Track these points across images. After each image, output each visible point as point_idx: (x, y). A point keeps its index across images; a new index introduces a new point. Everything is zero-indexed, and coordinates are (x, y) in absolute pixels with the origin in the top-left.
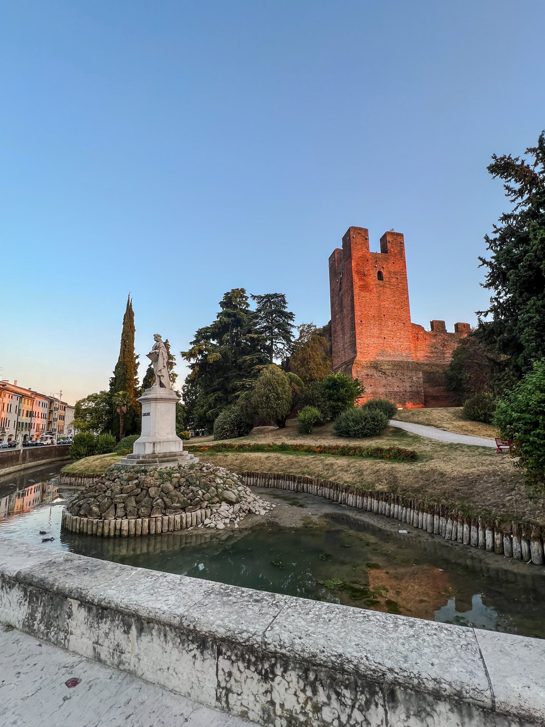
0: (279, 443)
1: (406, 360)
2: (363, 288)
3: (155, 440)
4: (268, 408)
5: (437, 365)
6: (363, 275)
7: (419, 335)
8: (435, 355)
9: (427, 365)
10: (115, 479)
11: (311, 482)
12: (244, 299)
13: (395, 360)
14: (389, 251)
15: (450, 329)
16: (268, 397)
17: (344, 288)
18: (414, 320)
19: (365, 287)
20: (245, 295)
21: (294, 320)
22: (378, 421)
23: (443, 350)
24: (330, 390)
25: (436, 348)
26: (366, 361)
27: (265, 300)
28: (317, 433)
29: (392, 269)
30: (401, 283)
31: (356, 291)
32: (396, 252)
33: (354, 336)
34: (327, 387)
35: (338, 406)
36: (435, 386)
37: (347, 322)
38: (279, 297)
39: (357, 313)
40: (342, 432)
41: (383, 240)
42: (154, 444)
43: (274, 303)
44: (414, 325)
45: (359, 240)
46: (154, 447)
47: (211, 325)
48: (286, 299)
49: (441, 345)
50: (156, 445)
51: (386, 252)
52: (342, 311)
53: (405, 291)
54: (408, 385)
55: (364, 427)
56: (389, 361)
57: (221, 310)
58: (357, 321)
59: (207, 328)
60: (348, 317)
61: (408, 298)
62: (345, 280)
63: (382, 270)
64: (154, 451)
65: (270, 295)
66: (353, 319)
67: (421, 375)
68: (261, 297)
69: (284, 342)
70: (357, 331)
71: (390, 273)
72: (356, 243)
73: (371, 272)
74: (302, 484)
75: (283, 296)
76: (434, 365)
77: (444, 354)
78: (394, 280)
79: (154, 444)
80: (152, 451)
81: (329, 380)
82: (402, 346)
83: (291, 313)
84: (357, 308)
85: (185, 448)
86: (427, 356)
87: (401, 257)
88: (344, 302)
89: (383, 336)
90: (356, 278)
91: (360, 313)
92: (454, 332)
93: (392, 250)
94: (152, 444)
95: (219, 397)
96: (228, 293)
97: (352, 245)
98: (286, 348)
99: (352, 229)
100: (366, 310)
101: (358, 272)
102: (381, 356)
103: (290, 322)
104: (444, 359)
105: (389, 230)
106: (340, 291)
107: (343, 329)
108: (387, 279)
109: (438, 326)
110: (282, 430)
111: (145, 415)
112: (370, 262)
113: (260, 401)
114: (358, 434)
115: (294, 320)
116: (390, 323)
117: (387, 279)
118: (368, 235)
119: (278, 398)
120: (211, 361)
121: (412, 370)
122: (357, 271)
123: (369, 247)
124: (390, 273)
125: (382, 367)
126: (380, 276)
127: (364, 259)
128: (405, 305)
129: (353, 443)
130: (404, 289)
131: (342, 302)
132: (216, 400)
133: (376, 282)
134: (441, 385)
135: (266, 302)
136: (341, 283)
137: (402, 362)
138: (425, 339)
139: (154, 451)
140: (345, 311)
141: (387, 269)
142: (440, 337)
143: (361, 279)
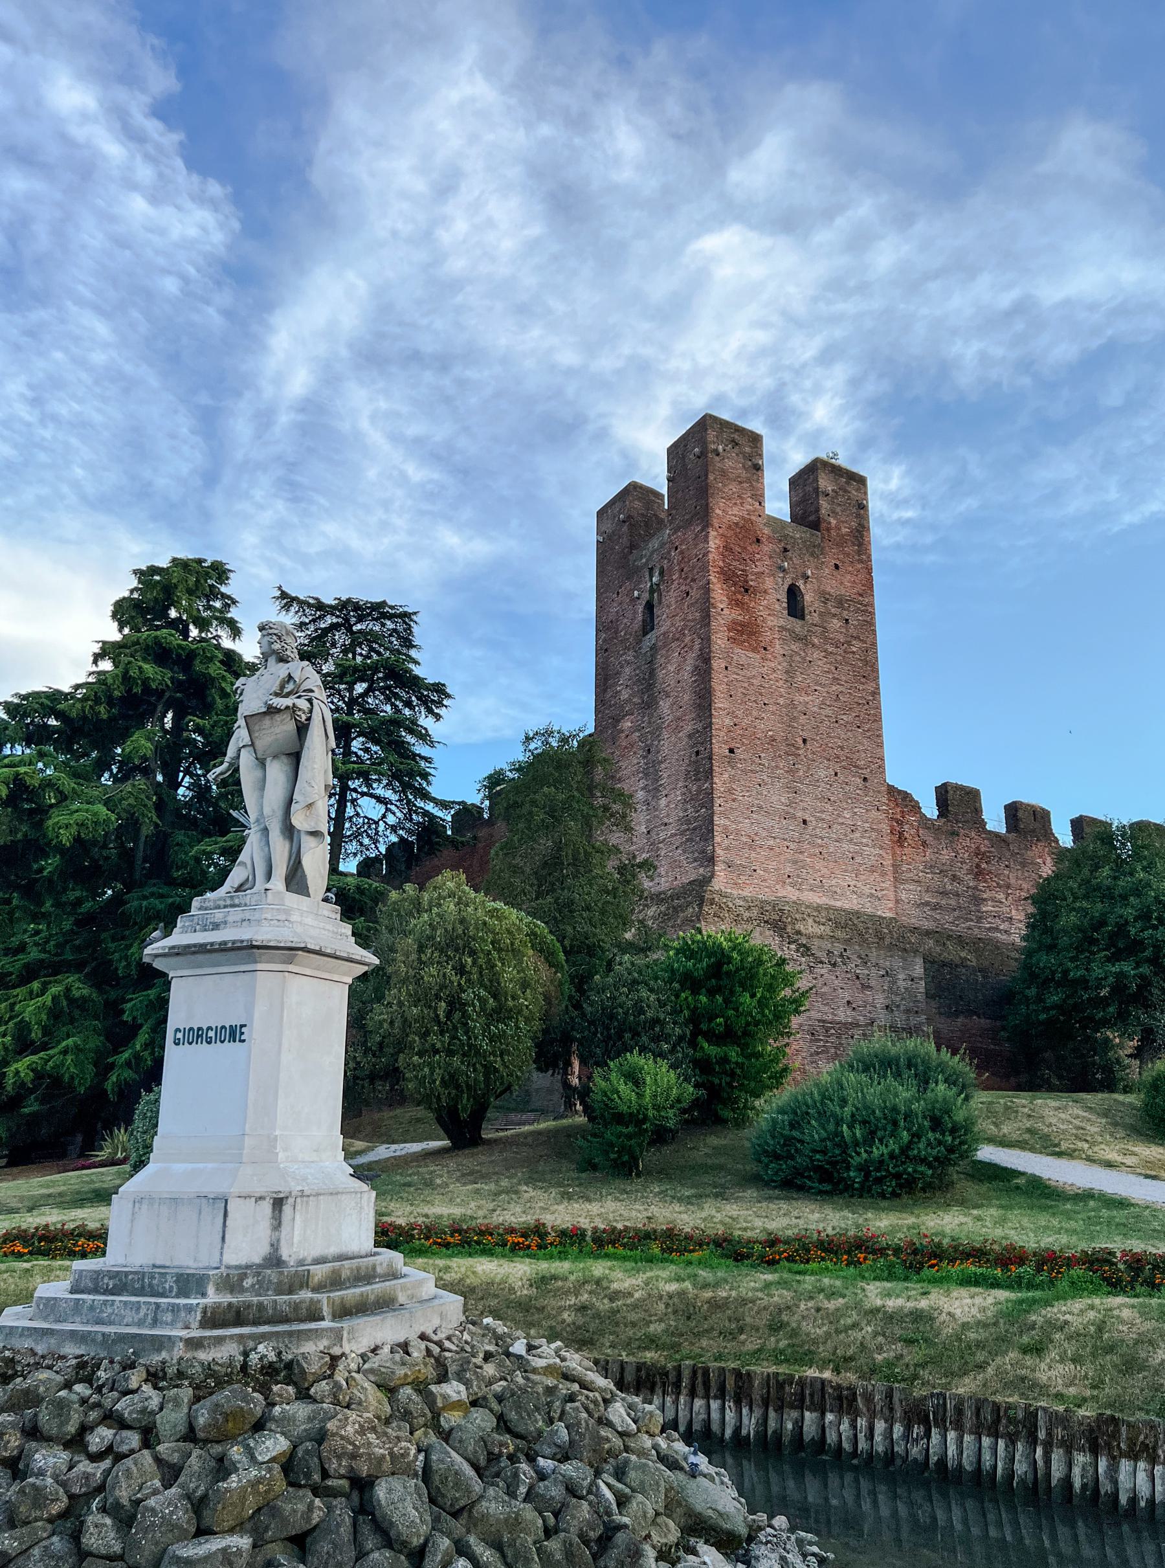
0: (514, 1215)
1: (869, 910)
2: (741, 633)
3: (283, 1188)
4: (450, 1053)
5: (960, 940)
6: (743, 589)
7: (906, 827)
8: (953, 902)
9: (928, 933)
10: (85, 1429)
11: (846, 1402)
12: (218, 604)
13: (838, 904)
14: (823, 525)
15: (995, 820)
16: (455, 1004)
17: (665, 623)
18: (895, 777)
19: (746, 632)
20: (223, 589)
21: (438, 717)
22: (953, 1131)
23: (975, 888)
24: (695, 992)
25: (954, 878)
26: (744, 899)
27: (330, 620)
28: (663, 1173)
29: (832, 586)
30: (857, 638)
31: (720, 640)
32: (845, 530)
33: (706, 800)
34: (691, 982)
35: (725, 1060)
36: (957, 1014)
37: (673, 747)
38: (391, 617)
39: (721, 720)
40: (798, 1173)
41: (805, 483)
42: (278, 1203)
43: (370, 638)
44: (891, 790)
45: (732, 463)
46: (277, 1225)
47: (77, 687)
48: (415, 629)
49: (970, 872)
50: (287, 1209)
51: (815, 525)
52: (649, 705)
53: (868, 670)
54: (880, 1000)
55: (905, 1150)
56: (818, 909)
57: (112, 633)
58: (719, 748)
59: (55, 696)
60: (678, 729)
61: (876, 693)
62: (671, 597)
63: (800, 583)
64: (275, 1246)
65: (357, 607)
66: (702, 736)
67: (918, 969)
68: (320, 606)
69: (389, 794)
70: (720, 781)
71: (825, 597)
72: (724, 473)
73: (769, 583)
74: (795, 1414)
75: (405, 616)
76: (949, 937)
77: (978, 901)
78: (836, 623)
79: (278, 1203)
80: (264, 1250)
81: (686, 951)
82: (858, 859)
83: (439, 689)
84: (720, 703)
85: (388, 1236)
86: (927, 904)
87: (859, 553)
88: (661, 674)
89: (799, 814)
90: (719, 594)
91: (728, 721)
92: (1002, 829)
93: (833, 522)
94: (267, 1207)
95: (72, 1001)
96: (153, 570)
97: (711, 477)
98: (391, 819)
99: (706, 425)
100: (748, 713)
101: (728, 576)
102: (793, 885)
103: (425, 721)
104: (979, 919)
105: (823, 456)
106: (645, 634)
107: (651, 772)
108: (816, 618)
109: (957, 802)
110: (469, 1160)
111: (198, 1035)
112: (767, 548)
113: (420, 1019)
114: (879, 1181)
115: (438, 717)
116: (822, 773)
117: (816, 618)
118: (761, 456)
119: (501, 1013)
120: (66, 837)
121: (891, 947)
122: (722, 572)
123: (762, 495)
124: (825, 597)
125: (800, 926)
126: (794, 604)
127: (747, 534)
128: (866, 714)
129: (886, 1223)
130: (866, 663)
131: (652, 673)
132: (55, 1013)
133: (782, 622)
134: (975, 1013)
135: (334, 627)
136: (650, 607)
137: (857, 914)
138: (924, 844)
139: (275, 1246)
140: (664, 705)
141: (822, 582)
142: (968, 842)
143: (736, 603)
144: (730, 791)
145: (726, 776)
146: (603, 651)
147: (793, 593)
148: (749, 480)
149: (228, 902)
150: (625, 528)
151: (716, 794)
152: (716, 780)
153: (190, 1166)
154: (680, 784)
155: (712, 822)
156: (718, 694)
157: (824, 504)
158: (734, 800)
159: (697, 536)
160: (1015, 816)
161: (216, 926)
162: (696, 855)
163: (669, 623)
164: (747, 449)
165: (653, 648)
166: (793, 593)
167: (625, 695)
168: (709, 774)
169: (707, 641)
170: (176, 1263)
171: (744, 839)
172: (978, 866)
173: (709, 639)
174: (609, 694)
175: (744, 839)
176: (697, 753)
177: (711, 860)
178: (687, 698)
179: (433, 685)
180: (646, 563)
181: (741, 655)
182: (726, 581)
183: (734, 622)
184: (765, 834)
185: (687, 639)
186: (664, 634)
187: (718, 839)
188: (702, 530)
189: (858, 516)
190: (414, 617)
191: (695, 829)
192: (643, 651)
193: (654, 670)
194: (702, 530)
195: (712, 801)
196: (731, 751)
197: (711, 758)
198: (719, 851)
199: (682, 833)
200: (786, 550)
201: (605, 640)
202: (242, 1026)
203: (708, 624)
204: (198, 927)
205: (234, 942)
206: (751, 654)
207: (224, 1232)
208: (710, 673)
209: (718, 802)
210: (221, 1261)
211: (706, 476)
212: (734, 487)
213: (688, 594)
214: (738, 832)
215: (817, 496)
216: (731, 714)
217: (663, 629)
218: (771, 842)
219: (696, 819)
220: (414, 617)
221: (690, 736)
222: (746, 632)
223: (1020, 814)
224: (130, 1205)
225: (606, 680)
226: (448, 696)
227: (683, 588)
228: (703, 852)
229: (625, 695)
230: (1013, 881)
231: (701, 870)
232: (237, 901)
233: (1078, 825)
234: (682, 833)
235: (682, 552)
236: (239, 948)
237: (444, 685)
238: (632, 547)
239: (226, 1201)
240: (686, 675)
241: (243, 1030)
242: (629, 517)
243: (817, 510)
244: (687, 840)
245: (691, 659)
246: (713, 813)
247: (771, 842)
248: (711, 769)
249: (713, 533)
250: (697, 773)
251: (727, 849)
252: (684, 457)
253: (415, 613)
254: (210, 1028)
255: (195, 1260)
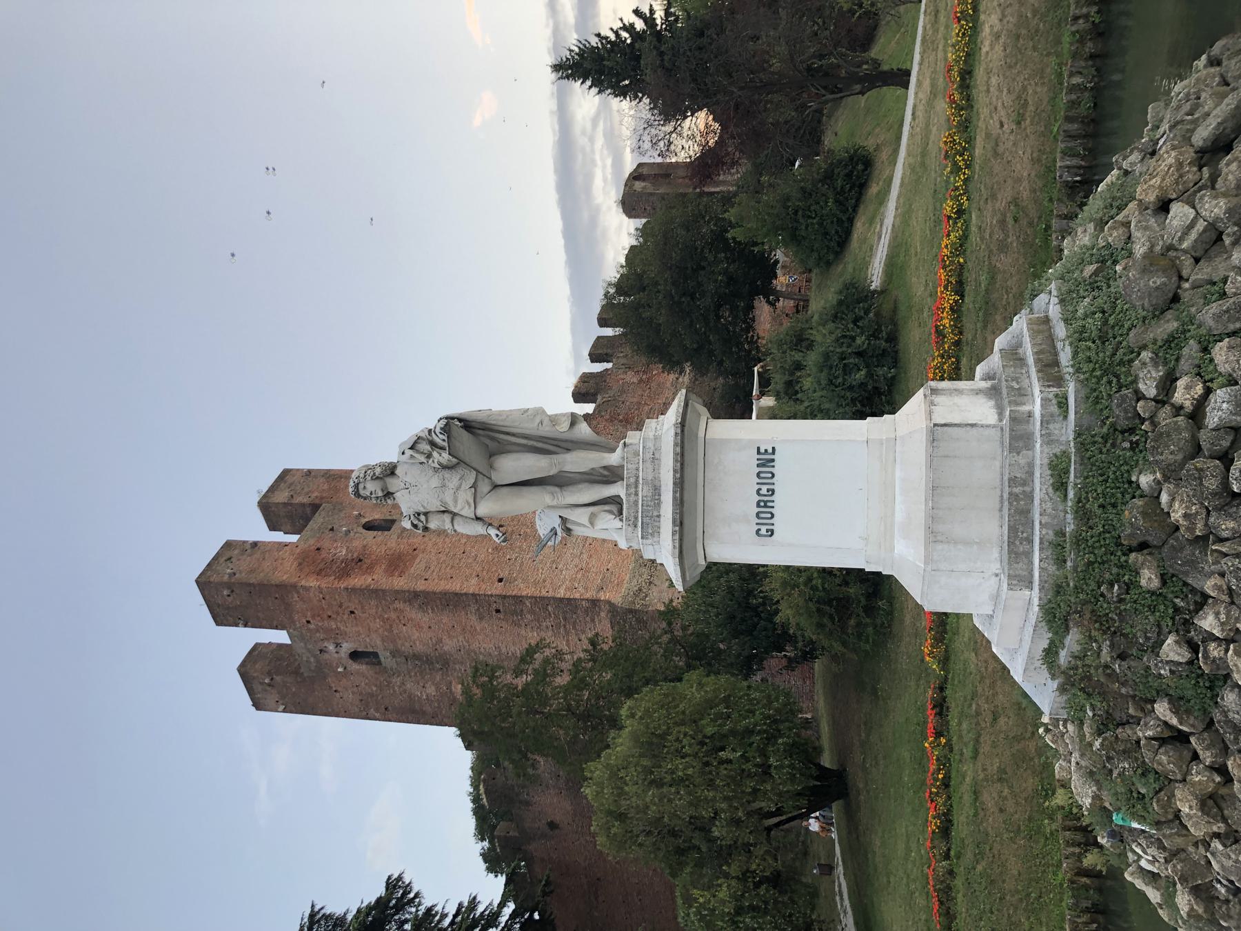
14: (317, 502)
31: (399, 583)
33: (542, 602)
39: (472, 586)
58: (498, 589)
63: (364, 521)
73: (357, 544)
83: (393, 884)
84: (455, 586)
88: (419, 648)
91: (474, 581)
93: (316, 494)
112: (326, 544)
122: (340, 578)
131: (416, 657)
140: (449, 645)
143: (370, 569)
144: (536, 583)
145: (522, 586)
146: (388, 714)
147: (369, 527)
148: (264, 553)
149: (633, 490)
150: (278, 678)
151: (537, 594)
152: (524, 593)
153: (898, 498)
154: (523, 632)
155: (561, 600)
156: (448, 587)
157: (299, 499)
158: (544, 581)
159: (302, 599)
160: (584, 395)
161: (657, 490)
162: (588, 619)
163: (374, 636)
164: (236, 552)
165: (395, 653)
166: (369, 527)
167: (431, 690)
168: (518, 599)
169: (398, 594)
170: (998, 483)
171: (579, 576)
172: (621, 421)
173: (397, 592)
174: (428, 709)
175: (579, 576)
176: (498, 611)
177: (595, 602)
178: (446, 619)
179: (387, 889)
180: (315, 656)
181: (417, 567)
182: (348, 575)
183: (386, 571)
184: (577, 560)
185: (393, 615)
186: (383, 641)
187: (577, 596)
188: (298, 592)
189: (316, 477)
190: (316, 909)
191: (565, 619)
192: (395, 666)
193: (414, 655)
194: (298, 592)
195: (542, 598)
196: (500, 580)
197: (505, 597)
198: (588, 596)
199: (567, 633)
200: (332, 529)
201: (377, 710)
202: (759, 452)
203: (383, 591)
204: (655, 513)
205: (675, 471)
206: (418, 560)
207: (967, 425)
208: (428, 593)
209: (544, 593)
210: (994, 426)
211: (250, 585)
212: (267, 564)
213: (352, 612)
214: (573, 580)
215: (291, 504)
216: (467, 578)
217: (379, 642)
218: (585, 556)
219: (557, 617)
220: (316, 909)
221: (481, 618)
222: (397, 563)
223: (583, 391)
224: (939, 547)
225: (413, 711)
226: (400, 878)
227: (346, 617)
228: (586, 611)
229: (431, 690)
230: (635, 400)
231: (603, 614)
232: (632, 480)
233: (603, 322)
234: (567, 633)
235: (313, 617)
236: (682, 442)
237: (389, 878)
238: (297, 672)
239: (935, 425)
240: (424, 618)
241: (762, 450)
242: (269, 673)
243: (303, 505)
244: (574, 628)
245: (413, 614)
246: (554, 598)
247: (585, 556)
248: (514, 597)
249: (303, 583)
250: (514, 613)
251: (586, 589)
252: (228, 608)
253: (313, 906)
254: (758, 491)
255: (995, 459)
